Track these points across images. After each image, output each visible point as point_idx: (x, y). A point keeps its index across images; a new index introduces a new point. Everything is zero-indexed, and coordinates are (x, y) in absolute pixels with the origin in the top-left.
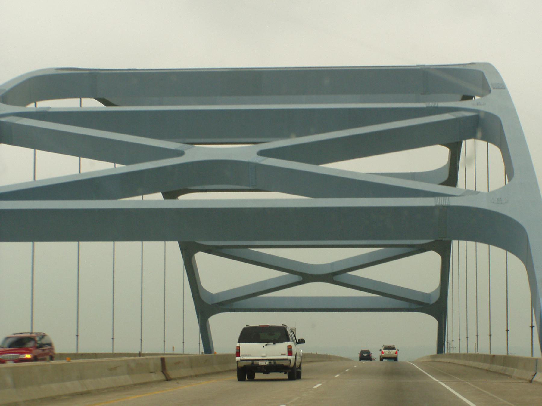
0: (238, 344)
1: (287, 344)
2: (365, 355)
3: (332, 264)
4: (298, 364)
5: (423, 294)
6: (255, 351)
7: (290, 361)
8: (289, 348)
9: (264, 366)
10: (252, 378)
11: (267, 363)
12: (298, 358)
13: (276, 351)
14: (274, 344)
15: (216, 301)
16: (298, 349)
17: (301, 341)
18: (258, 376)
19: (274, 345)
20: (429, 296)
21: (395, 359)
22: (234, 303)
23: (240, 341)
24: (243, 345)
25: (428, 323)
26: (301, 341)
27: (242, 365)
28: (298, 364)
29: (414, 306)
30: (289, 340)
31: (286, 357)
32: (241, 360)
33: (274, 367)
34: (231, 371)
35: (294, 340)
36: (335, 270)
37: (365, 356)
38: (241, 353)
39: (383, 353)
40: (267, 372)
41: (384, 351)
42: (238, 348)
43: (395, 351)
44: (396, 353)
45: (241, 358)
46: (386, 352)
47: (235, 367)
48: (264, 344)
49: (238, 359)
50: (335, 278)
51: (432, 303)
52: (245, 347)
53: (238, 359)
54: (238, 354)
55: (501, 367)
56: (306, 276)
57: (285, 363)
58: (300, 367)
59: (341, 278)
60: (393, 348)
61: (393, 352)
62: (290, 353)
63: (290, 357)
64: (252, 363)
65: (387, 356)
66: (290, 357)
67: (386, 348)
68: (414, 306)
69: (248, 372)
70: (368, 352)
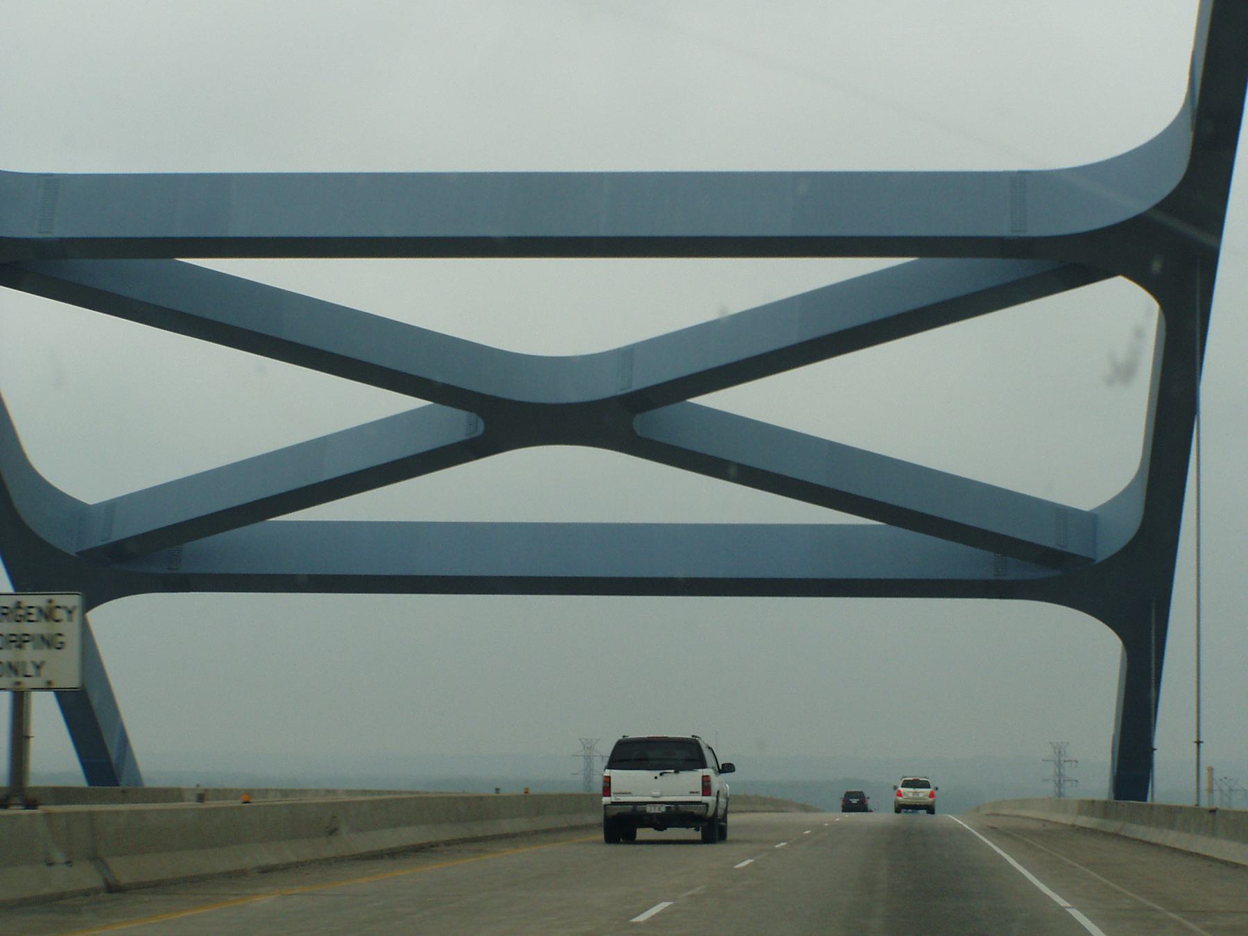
0: (607, 773)
1: (701, 772)
2: (854, 801)
3: (627, 355)
4: (720, 812)
5: (1063, 514)
6: (640, 786)
7: (707, 805)
8: (706, 781)
9: (657, 815)
10: (630, 839)
11: (663, 808)
12: (722, 800)
13: (680, 787)
14: (677, 772)
15: (96, 540)
16: (719, 782)
17: (728, 768)
18: (643, 833)
19: (675, 776)
20: (1089, 520)
21: (930, 809)
22: (190, 547)
23: (611, 765)
24: (616, 775)
25: (1085, 646)
26: (728, 768)
27: (615, 813)
28: (720, 812)
29: (1016, 571)
30: (704, 766)
31: (698, 798)
32: (613, 803)
33: (677, 815)
34: (587, 828)
35: (714, 764)
36: (638, 384)
37: (855, 803)
38: (613, 790)
39: (900, 794)
40: (660, 828)
41: (903, 790)
42: (608, 780)
43: (928, 791)
44: (932, 795)
45: (613, 799)
46: (908, 792)
47: (599, 818)
48: (657, 773)
49: (606, 800)
50: (643, 424)
51: (1100, 558)
52: (620, 778)
53: (606, 800)
54: (607, 791)
55: (1094, 820)
56: (497, 409)
57: (697, 810)
58: (724, 819)
59: (661, 422)
60: (926, 785)
61: (923, 793)
62: (706, 790)
63: (705, 799)
64: (634, 809)
65: (908, 802)
66: (705, 799)
67: (907, 784)
68: (1016, 571)
69: (623, 825)
70: (860, 795)
